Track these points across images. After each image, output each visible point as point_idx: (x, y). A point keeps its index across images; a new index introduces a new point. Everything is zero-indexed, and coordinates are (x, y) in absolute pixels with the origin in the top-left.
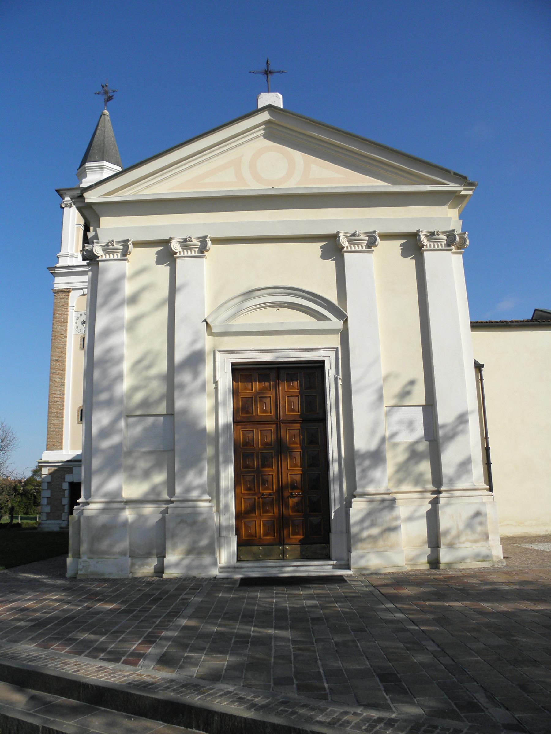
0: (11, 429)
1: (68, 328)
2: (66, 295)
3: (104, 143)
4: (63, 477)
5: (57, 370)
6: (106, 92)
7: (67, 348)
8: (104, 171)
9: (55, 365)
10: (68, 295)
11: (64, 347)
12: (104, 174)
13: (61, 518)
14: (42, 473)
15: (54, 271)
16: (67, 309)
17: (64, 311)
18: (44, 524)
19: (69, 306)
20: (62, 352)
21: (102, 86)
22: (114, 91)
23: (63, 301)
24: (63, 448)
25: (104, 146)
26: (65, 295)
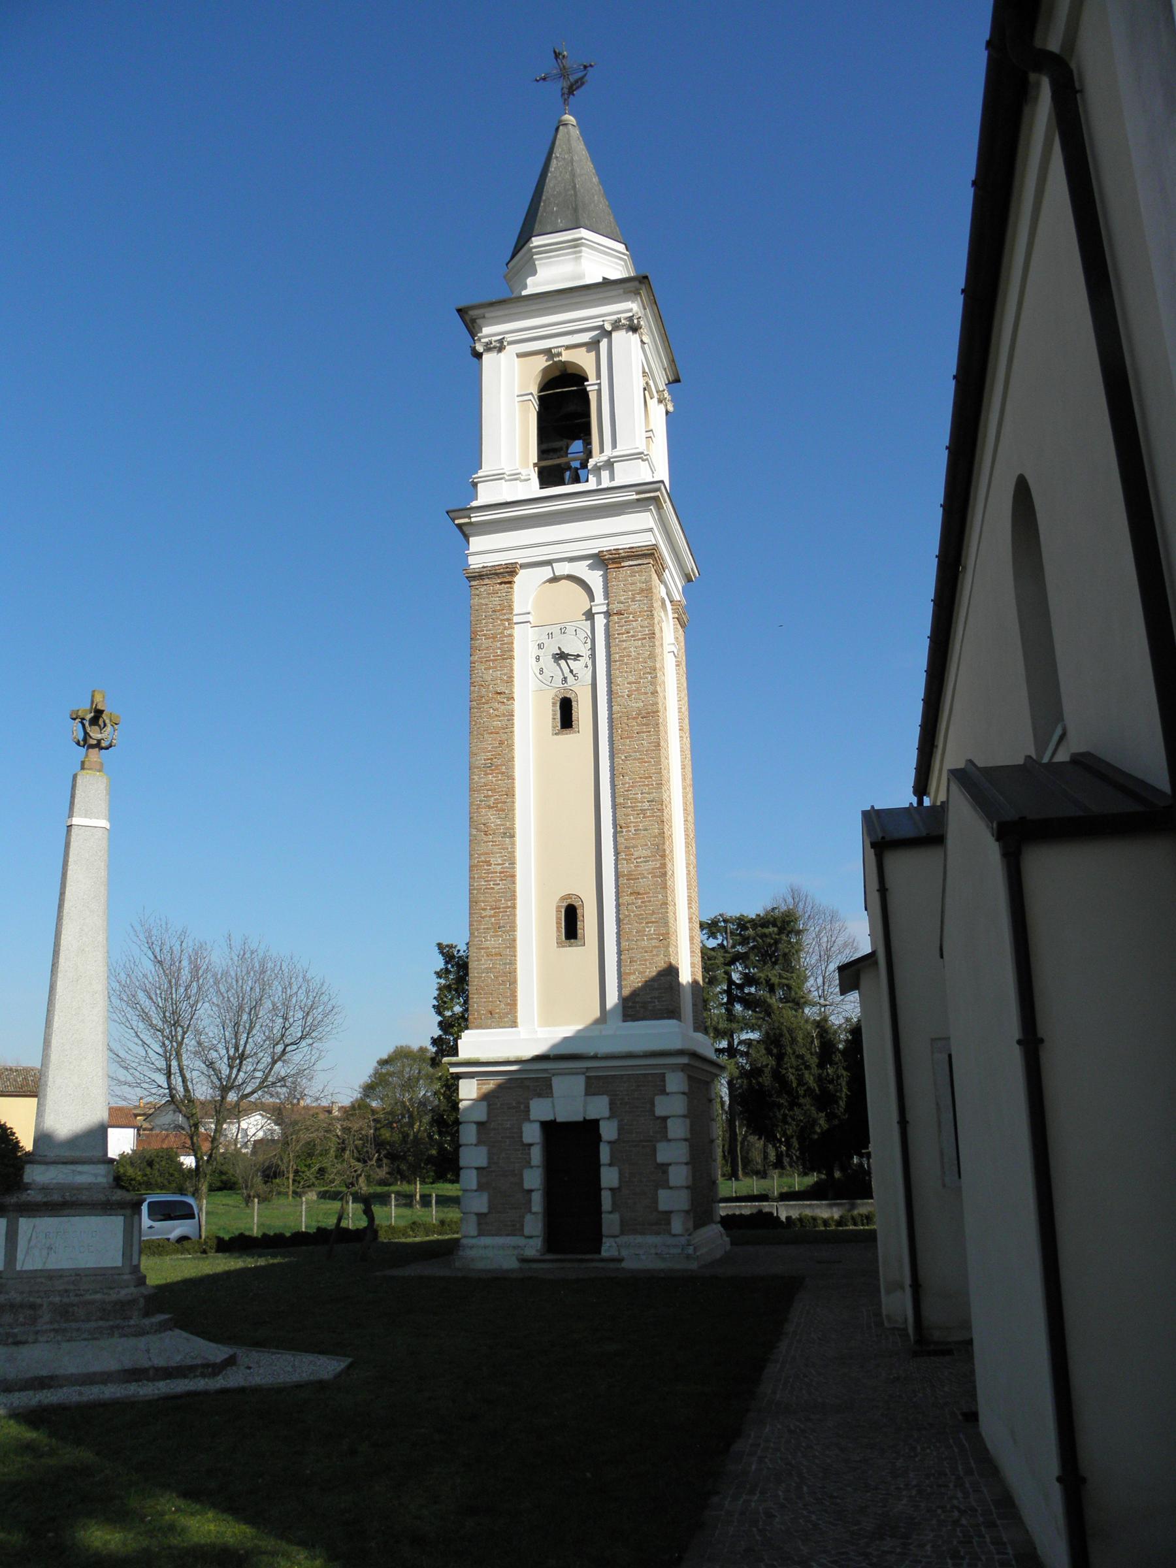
0: (326, 985)
1: (516, 674)
2: (505, 583)
3: (574, 187)
4: (522, 1107)
5: (490, 793)
6: (563, 73)
7: (517, 729)
8: (583, 254)
9: (483, 780)
10: (510, 583)
11: (508, 728)
12: (582, 260)
13: (522, 1230)
14: (461, 1096)
15: (466, 520)
16: (508, 620)
17: (501, 627)
18: (472, 1247)
19: (514, 613)
20: (501, 743)
21: (555, 52)
22: (585, 67)
23: (496, 600)
24: (519, 1020)
25: (576, 195)
26: (501, 583)
